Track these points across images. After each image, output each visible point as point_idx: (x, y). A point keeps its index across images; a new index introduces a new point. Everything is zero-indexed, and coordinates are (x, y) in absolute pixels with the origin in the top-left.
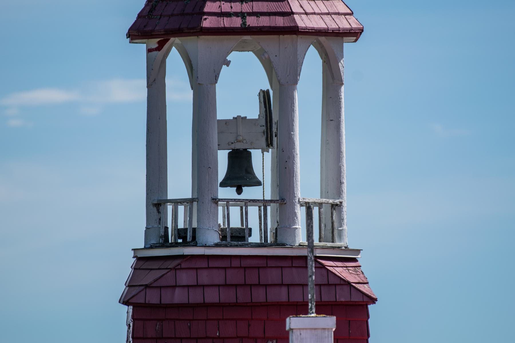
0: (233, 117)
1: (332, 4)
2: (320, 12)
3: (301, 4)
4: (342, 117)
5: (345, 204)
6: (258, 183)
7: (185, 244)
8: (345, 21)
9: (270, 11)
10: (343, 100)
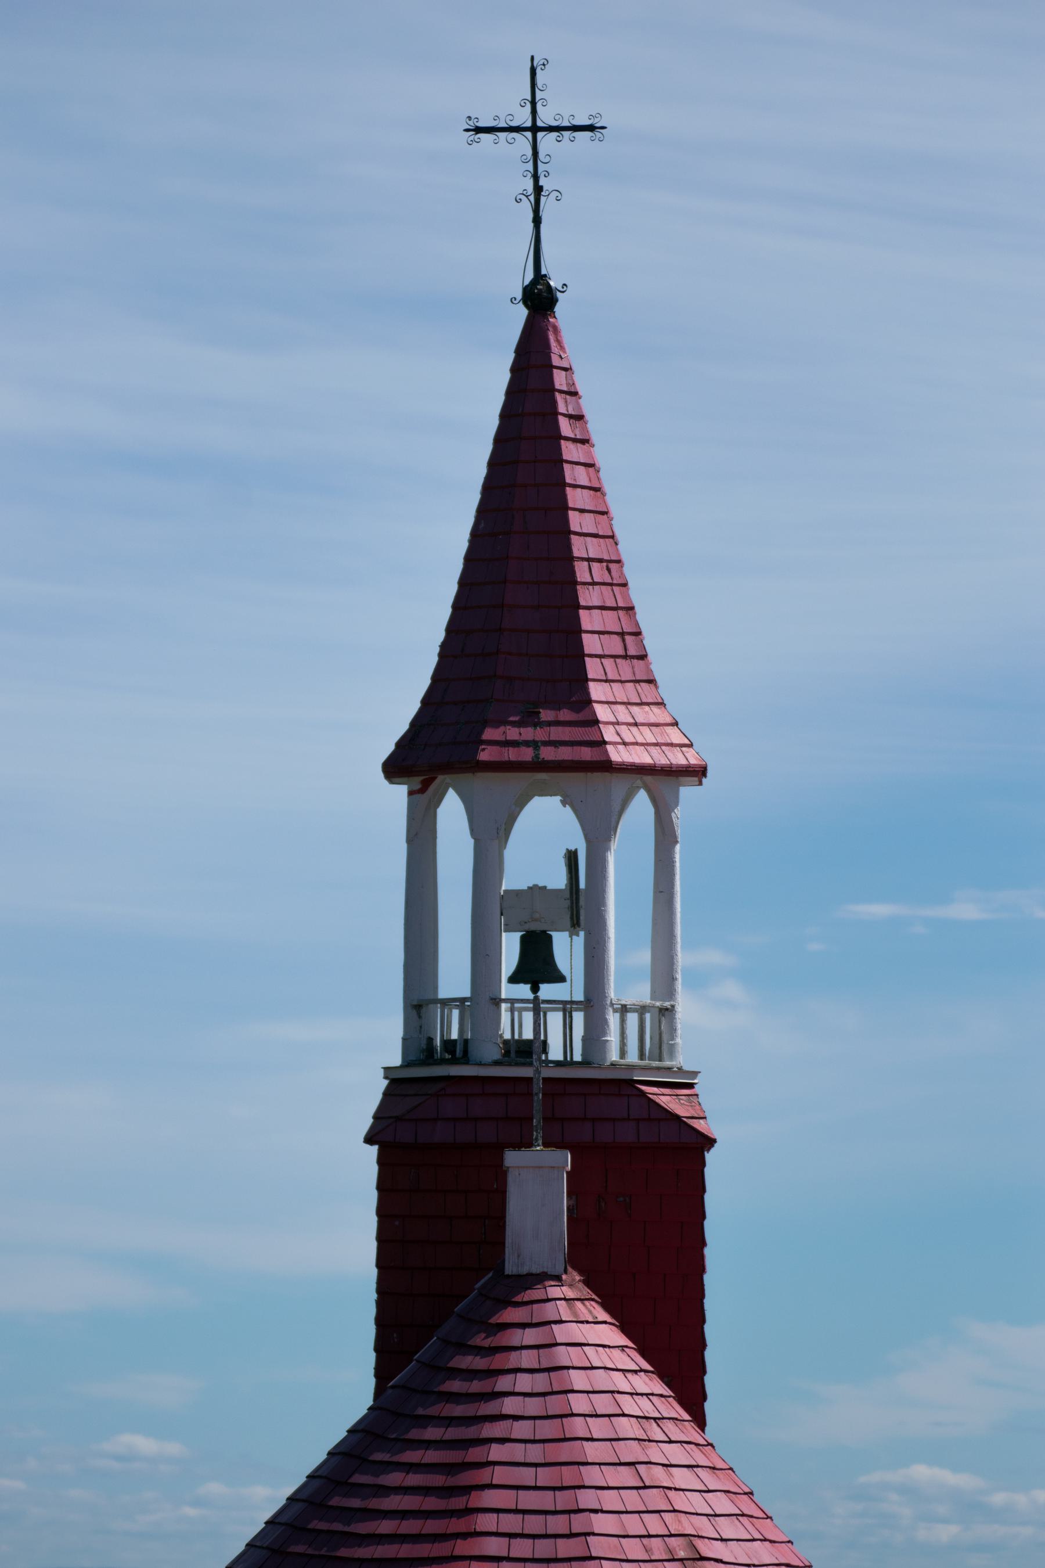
0: (528, 887)
1: (662, 732)
2: (644, 742)
3: (618, 730)
4: (675, 888)
5: (679, 1009)
6: (561, 979)
7: (454, 1061)
8: (680, 755)
9: (573, 740)
10: (678, 865)
